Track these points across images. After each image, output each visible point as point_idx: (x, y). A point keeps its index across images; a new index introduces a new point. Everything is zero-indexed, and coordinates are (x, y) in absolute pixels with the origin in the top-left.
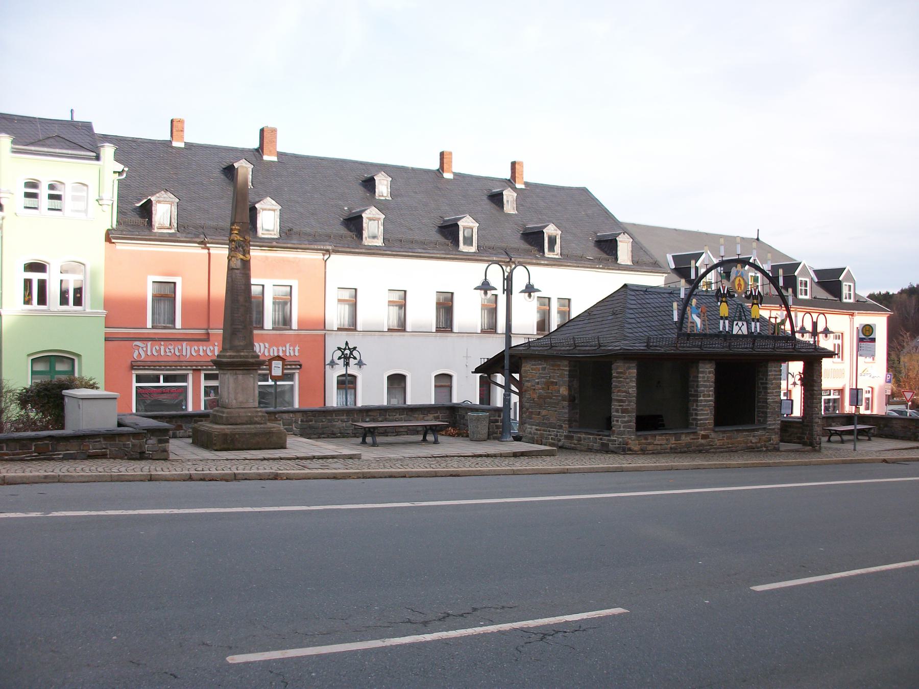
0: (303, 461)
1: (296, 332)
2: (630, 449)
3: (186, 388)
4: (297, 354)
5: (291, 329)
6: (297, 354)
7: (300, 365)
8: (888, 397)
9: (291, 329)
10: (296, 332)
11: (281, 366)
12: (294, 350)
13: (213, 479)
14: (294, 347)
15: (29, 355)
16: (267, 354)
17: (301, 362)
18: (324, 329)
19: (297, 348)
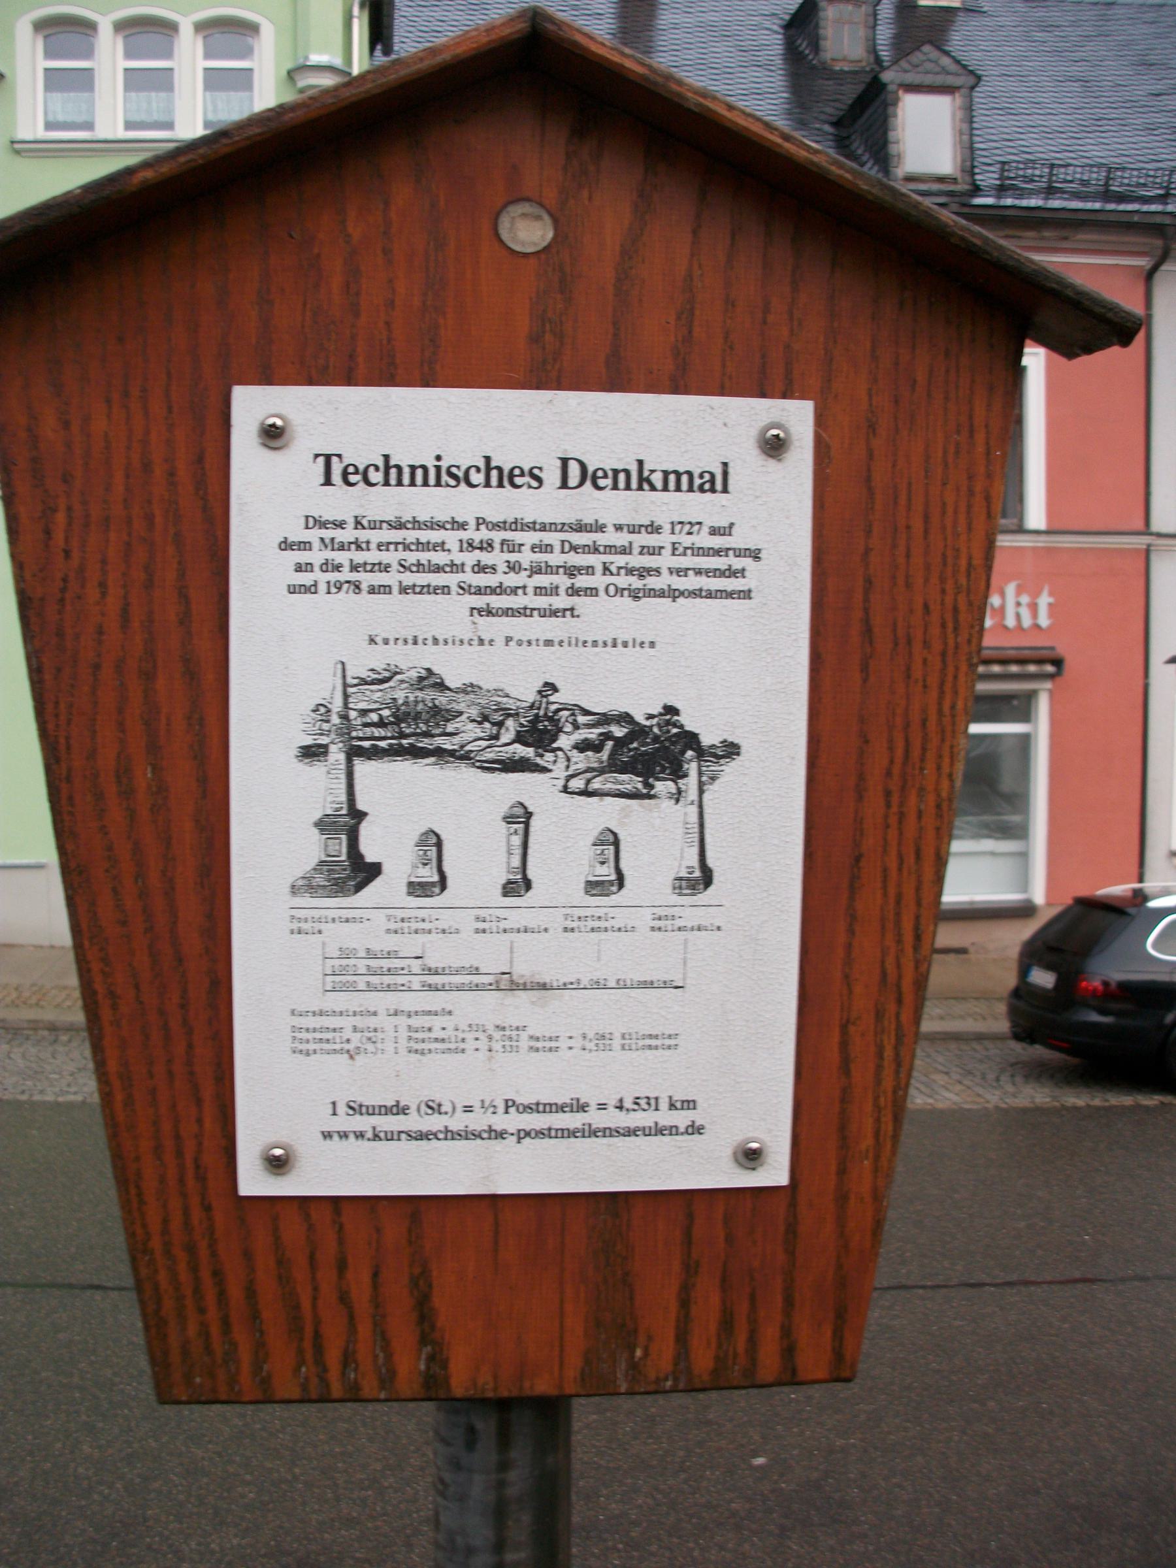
0: (1077, 1274)
1: (1042, 542)
2: (49, 1029)
3: (1025, 741)
4: (1044, 621)
5: (1021, 530)
6: (1044, 621)
7: (1058, 662)
8: (504, 887)
9: (1021, 530)
10: (1042, 542)
11: (746, 668)
12: (1034, 607)
13: (685, 1303)
14: (1036, 594)
15: (746, 594)
16: (1027, 622)
17: (1061, 650)
18: (1146, 530)
19: (1044, 600)
